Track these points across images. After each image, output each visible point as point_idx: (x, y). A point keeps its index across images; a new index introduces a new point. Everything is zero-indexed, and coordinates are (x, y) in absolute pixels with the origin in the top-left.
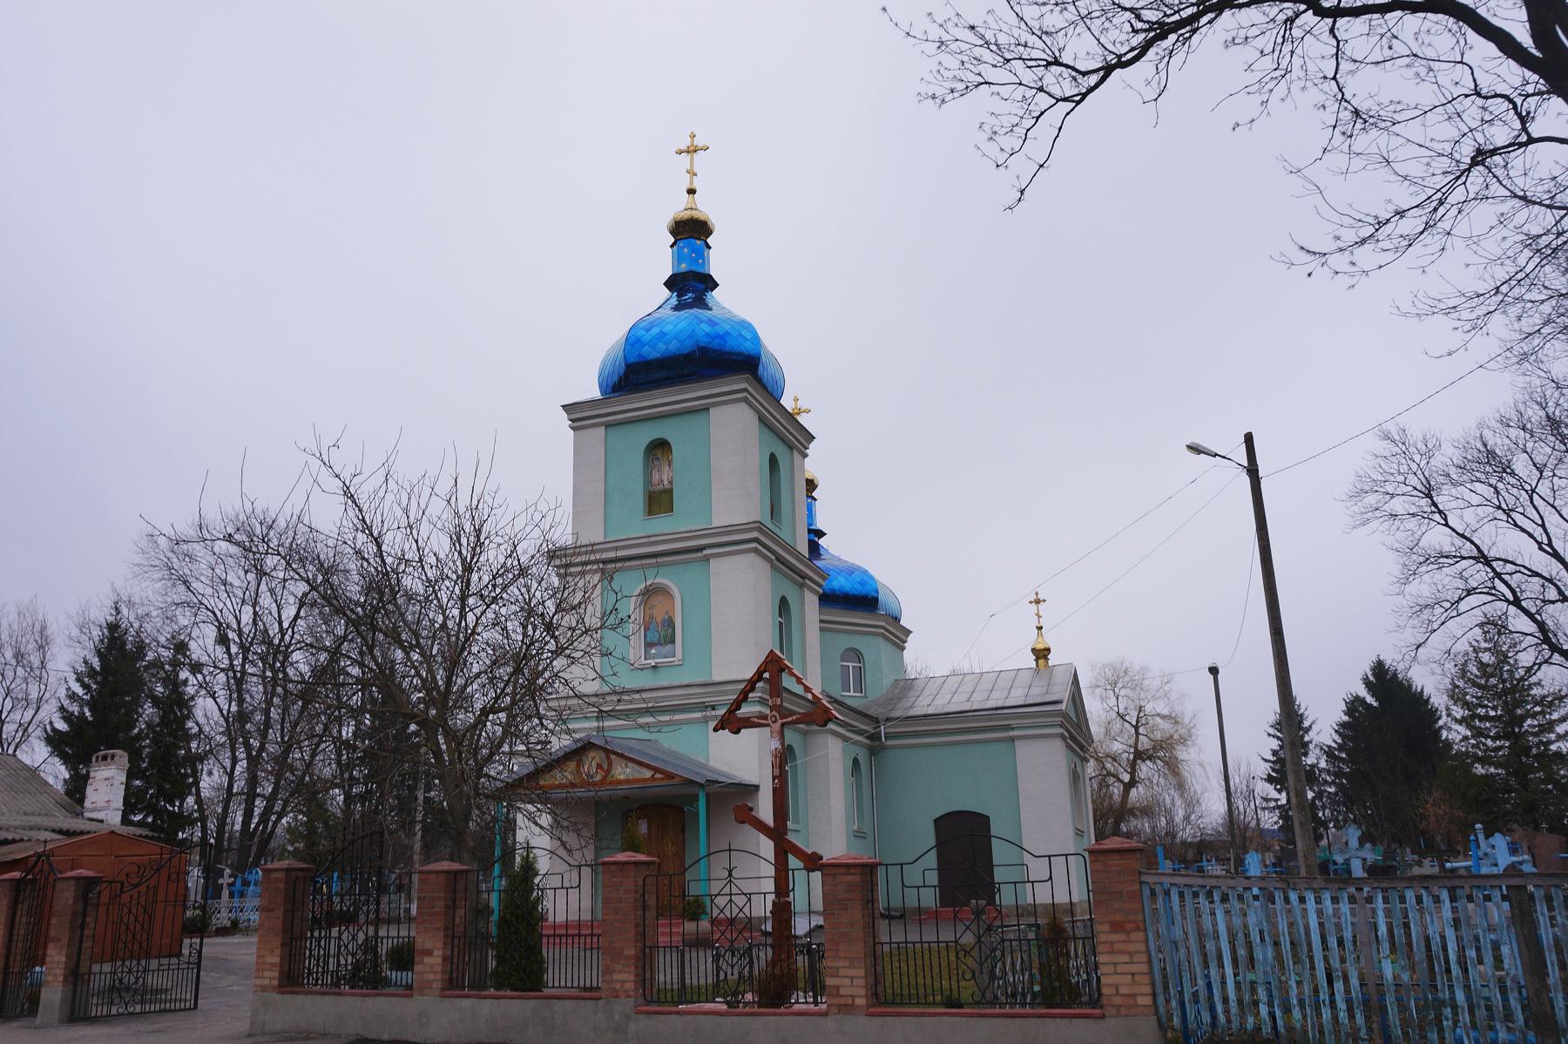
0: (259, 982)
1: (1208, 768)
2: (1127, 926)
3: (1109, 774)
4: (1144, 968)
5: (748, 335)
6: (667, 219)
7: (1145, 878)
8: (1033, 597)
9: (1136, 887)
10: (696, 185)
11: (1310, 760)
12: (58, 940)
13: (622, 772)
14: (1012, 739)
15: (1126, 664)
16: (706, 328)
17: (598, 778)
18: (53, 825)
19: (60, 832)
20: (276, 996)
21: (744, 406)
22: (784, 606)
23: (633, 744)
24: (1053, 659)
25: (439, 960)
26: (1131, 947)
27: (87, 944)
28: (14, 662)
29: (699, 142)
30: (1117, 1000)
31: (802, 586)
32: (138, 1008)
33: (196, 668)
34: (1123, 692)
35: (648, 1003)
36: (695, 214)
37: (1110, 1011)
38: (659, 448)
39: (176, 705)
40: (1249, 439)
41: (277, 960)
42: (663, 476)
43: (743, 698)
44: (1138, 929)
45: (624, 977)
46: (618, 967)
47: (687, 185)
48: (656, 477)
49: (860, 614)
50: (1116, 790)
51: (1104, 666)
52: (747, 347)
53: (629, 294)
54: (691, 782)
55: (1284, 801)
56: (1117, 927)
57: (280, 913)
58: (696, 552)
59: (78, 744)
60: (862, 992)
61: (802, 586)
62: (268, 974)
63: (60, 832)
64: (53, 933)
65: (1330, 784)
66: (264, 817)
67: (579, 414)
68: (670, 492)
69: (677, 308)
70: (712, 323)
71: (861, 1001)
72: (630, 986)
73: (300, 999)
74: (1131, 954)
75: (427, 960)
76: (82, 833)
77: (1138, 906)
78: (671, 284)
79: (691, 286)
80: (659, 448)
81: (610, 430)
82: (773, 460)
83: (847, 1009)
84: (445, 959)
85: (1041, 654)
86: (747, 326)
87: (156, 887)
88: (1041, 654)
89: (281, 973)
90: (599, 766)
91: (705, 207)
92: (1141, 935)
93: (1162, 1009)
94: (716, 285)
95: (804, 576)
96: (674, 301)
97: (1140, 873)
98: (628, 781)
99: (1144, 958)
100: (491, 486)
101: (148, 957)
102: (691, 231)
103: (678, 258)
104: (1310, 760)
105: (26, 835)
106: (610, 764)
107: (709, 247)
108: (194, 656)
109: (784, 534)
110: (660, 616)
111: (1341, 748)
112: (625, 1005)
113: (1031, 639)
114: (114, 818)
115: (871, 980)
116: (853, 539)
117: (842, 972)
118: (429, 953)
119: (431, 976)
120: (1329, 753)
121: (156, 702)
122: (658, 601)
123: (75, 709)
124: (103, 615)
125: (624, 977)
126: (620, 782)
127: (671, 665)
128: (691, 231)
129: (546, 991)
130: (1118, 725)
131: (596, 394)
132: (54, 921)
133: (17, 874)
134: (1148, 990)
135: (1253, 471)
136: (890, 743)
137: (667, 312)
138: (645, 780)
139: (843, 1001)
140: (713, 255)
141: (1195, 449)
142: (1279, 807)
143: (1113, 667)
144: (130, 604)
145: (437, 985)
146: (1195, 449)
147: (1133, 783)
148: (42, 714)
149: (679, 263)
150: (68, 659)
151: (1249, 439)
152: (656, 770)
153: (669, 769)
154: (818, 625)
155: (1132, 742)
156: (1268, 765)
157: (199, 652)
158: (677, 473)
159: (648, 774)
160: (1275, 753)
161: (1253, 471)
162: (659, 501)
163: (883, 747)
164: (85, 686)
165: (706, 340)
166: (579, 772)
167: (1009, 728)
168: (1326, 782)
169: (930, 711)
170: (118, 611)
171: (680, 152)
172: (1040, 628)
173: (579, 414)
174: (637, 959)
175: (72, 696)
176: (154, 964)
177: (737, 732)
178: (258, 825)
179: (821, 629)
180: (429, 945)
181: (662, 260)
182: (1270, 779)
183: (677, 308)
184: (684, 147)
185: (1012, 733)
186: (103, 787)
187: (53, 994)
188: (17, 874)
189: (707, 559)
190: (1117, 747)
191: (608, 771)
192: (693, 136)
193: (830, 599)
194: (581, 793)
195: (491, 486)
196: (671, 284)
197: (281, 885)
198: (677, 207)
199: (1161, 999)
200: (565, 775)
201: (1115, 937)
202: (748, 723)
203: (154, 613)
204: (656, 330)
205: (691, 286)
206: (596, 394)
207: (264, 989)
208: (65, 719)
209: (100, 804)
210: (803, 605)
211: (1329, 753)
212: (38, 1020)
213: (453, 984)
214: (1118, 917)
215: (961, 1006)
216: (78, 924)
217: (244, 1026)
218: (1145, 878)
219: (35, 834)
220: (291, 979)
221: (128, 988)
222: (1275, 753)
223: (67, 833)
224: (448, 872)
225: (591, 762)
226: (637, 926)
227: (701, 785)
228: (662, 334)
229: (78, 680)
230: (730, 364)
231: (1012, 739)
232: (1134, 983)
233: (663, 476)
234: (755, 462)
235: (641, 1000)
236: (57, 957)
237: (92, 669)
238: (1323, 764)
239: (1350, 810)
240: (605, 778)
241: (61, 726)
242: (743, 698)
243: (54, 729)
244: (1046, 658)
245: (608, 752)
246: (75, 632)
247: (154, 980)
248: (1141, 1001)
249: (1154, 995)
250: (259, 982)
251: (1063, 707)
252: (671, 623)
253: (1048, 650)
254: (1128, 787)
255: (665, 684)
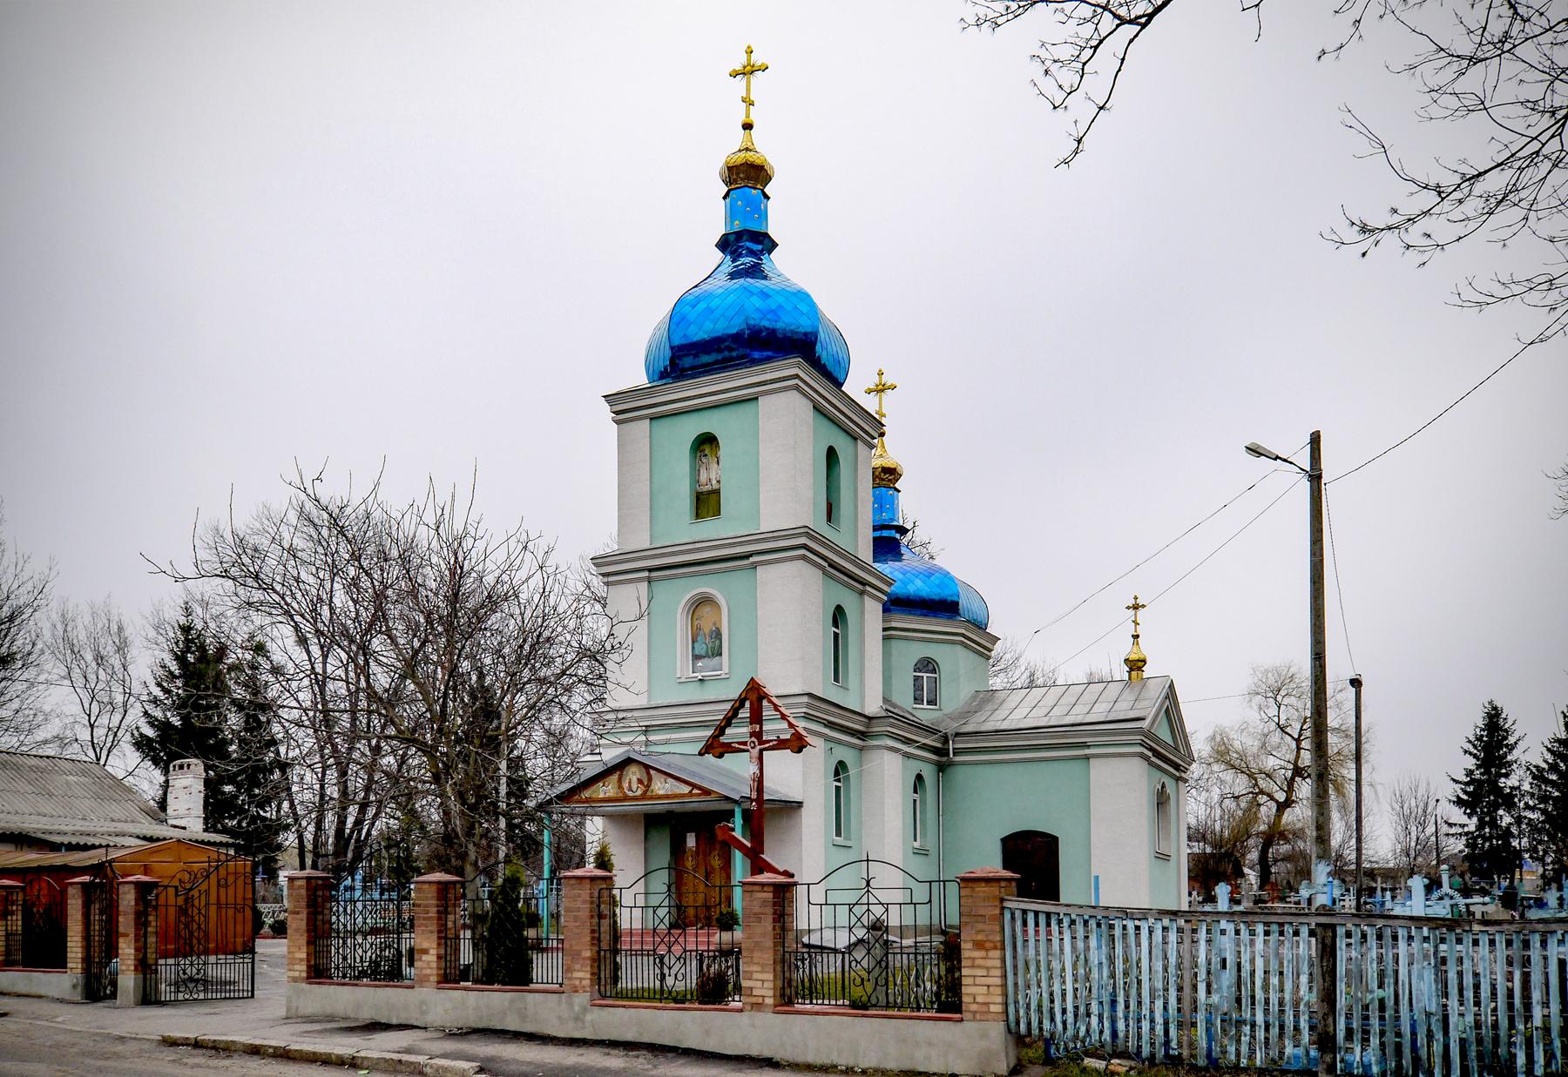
0: (291, 974)
1: (1379, 788)
2: (988, 945)
3: (1262, 792)
4: (998, 981)
5: (803, 308)
6: (718, 164)
7: (1007, 904)
8: (1131, 602)
9: (997, 911)
10: (754, 118)
11: (1512, 781)
12: (126, 935)
13: (661, 786)
14: (1087, 758)
15: (1292, 670)
16: (756, 302)
17: (639, 793)
18: (138, 831)
19: (145, 838)
20: (305, 986)
21: (794, 394)
22: (838, 616)
23: (677, 760)
24: (1148, 671)
25: (434, 958)
26: (989, 963)
27: (152, 939)
28: (94, 664)
29: (757, 59)
30: (974, 1007)
31: (862, 593)
32: (202, 996)
33: (277, 671)
34: (1286, 701)
35: (604, 997)
36: (751, 157)
37: (966, 1015)
38: (706, 443)
39: (258, 710)
40: (1315, 440)
41: (304, 956)
42: (711, 475)
43: (728, 721)
44: (995, 948)
45: (580, 975)
46: (577, 967)
47: (742, 119)
48: (703, 477)
49: (934, 620)
50: (1267, 810)
51: (1267, 671)
52: (804, 325)
53: (681, 259)
54: (727, 798)
55: (1472, 828)
56: (979, 945)
57: (304, 916)
58: (741, 558)
59: (164, 747)
60: (771, 993)
61: (862, 593)
62: (297, 967)
63: (145, 838)
64: (121, 929)
65: (1532, 809)
66: (358, 823)
67: (624, 406)
68: (717, 492)
69: (733, 276)
70: (764, 295)
71: (769, 1001)
72: (587, 982)
73: (325, 988)
74: (988, 968)
75: (425, 957)
76: (158, 840)
77: (998, 928)
78: (724, 244)
79: (746, 245)
80: (706, 443)
81: (655, 423)
82: (831, 454)
83: (758, 1006)
84: (439, 957)
85: (1135, 665)
86: (803, 296)
87: (207, 892)
88: (1135, 665)
89: (309, 967)
90: (640, 781)
91: (767, 149)
92: (997, 953)
93: (1012, 1017)
94: (774, 245)
95: (864, 583)
96: (728, 266)
97: (1002, 900)
98: (667, 797)
99: (998, 972)
100: (474, 517)
101: (207, 952)
102: (747, 176)
103: (731, 214)
104: (1512, 781)
105: (113, 840)
106: (650, 779)
107: (767, 197)
108: (274, 658)
109: (841, 539)
110: (707, 627)
111: (1553, 768)
112: (582, 999)
113: (1125, 649)
114: (195, 826)
115: (780, 984)
116: (950, 537)
117: (755, 976)
118: (425, 952)
119: (428, 971)
120: (1538, 776)
121: (239, 706)
122: (706, 610)
123: (158, 713)
124: (176, 616)
125: (580, 975)
126: (660, 797)
127: (718, 679)
128: (747, 176)
129: (532, 986)
130: (1276, 737)
131: (640, 379)
132: (121, 919)
133: (86, 878)
134: (999, 999)
135: (1315, 478)
136: (958, 759)
137: (721, 282)
138: (683, 796)
139: (754, 1000)
140: (772, 207)
141: (1255, 451)
142: (1467, 834)
143: (1277, 670)
144: (205, 605)
145: (434, 979)
146: (1255, 451)
147: (1288, 803)
148: (129, 719)
149: (732, 222)
150: (148, 662)
151: (1315, 440)
152: (694, 786)
153: (705, 785)
154: (880, 634)
155: (1292, 757)
156: (1458, 787)
157: (279, 652)
158: (722, 473)
159: (686, 789)
160: (1470, 773)
161: (1315, 478)
162: (706, 503)
163: (951, 764)
164: (167, 691)
165: (756, 316)
166: (620, 787)
167: (1085, 745)
168: (1527, 807)
169: (1005, 726)
170: (188, 611)
171: (734, 74)
172: (1136, 637)
173: (624, 406)
174: (593, 960)
175: (155, 701)
176: (212, 959)
177: (721, 756)
178: (352, 832)
179: (885, 638)
180: (425, 945)
181: (712, 216)
182: (1459, 802)
183: (733, 276)
184: (739, 68)
185: (1087, 751)
186: (182, 795)
187: (128, 981)
188: (86, 878)
189: (754, 566)
190: (1271, 763)
191: (648, 786)
192: (750, 52)
193: (897, 604)
194: (627, 807)
195: (474, 517)
196: (724, 244)
197: (303, 892)
198: (728, 146)
199: (1011, 1009)
200: (607, 789)
201: (977, 954)
202: (729, 748)
203: (229, 613)
204: (702, 306)
205: (746, 245)
206: (640, 379)
207: (295, 980)
208: (151, 724)
209: (182, 811)
210: (863, 613)
211: (1538, 776)
212: (118, 1002)
213: (452, 976)
214: (980, 937)
215: (866, 1008)
216: (141, 921)
217: (283, 1013)
218: (1007, 904)
219: (120, 841)
220: (318, 972)
221: (191, 979)
222: (1470, 773)
223: (151, 839)
224: (439, 883)
225: (633, 774)
226: (593, 931)
227: (735, 802)
228: (710, 310)
229: (159, 685)
230: (787, 345)
231: (1087, 758)
232: (989, 994)
233: (711, 475)
234: (810, 462)
235: (597, 995)
236: (127, 949)
237: (171, 673)
238: (1526, 787)
239: (1553, 838)
240: (645, 792)
241: (150, 732)
242: (728, 721)
243: (141, 735)
244: (1140, 669)
245: (647, 767)
246: (152, 634)
247: (212, 972)
248: (993, 1008)
249: (1006, 1004)
250: (291, 974)
251: (1145, 724)
252: (718, 634)
253: (1144, 661)
254: (1283, 807)
255: (712, 698)
